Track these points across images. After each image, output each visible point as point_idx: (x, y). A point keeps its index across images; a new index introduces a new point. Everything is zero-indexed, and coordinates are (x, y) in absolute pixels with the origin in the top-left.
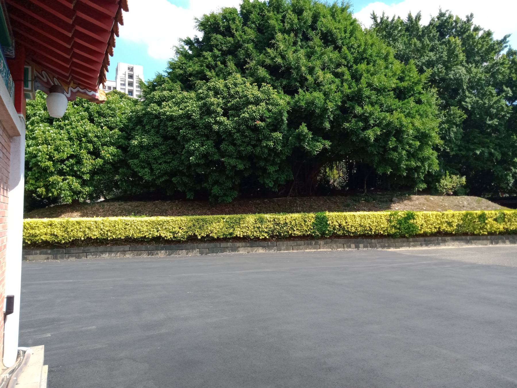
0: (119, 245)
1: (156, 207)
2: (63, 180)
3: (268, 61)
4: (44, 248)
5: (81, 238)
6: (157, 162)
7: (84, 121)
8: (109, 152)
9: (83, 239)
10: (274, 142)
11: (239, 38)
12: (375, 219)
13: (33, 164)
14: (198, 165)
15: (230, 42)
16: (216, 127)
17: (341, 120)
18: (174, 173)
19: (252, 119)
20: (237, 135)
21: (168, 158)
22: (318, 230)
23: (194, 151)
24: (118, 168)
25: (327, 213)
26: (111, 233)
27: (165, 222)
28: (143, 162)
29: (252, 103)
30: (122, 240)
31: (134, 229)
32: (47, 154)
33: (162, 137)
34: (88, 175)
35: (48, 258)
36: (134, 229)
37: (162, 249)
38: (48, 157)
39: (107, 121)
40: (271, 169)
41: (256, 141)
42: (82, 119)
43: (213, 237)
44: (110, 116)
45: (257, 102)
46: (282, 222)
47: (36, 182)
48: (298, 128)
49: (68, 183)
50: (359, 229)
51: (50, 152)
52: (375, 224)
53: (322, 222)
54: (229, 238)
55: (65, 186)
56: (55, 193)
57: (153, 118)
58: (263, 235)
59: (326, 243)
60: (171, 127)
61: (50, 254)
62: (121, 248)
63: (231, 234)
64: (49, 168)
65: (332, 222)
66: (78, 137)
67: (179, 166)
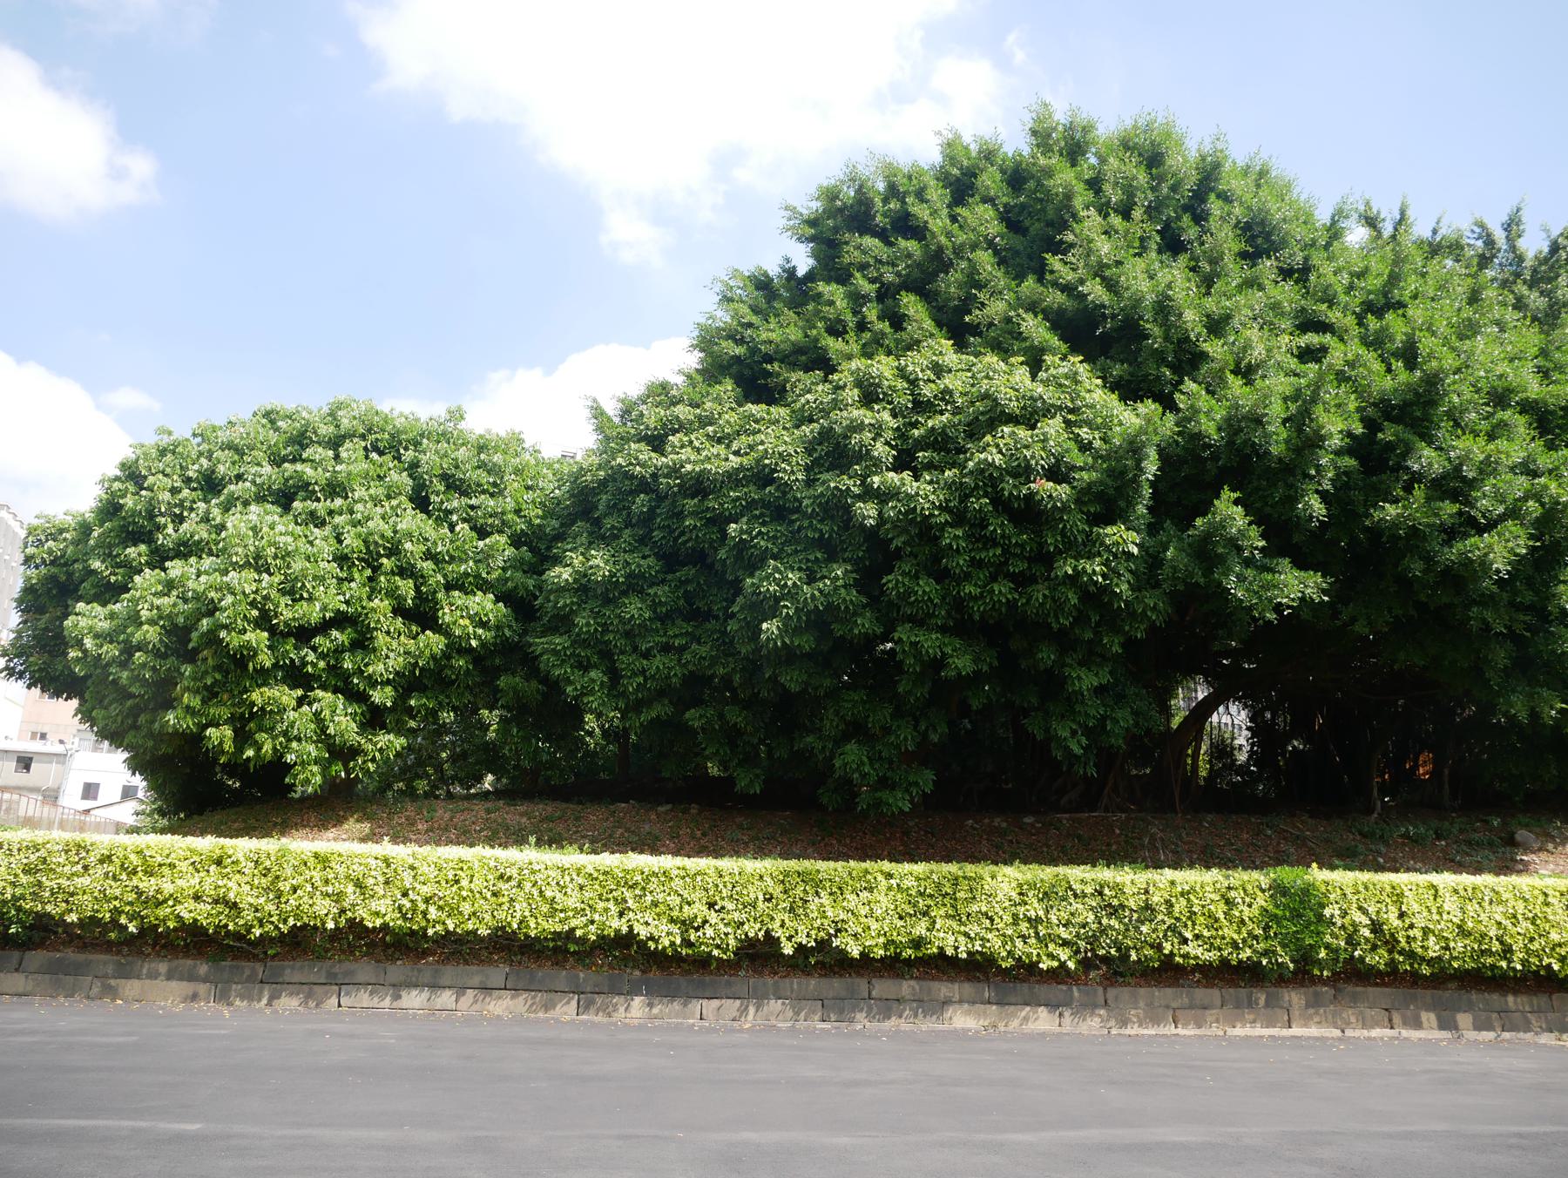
0: (467, 963)
1: (619, 824)
2: (301, 702)
3: (1056, 298)
4: (186, 951)
5: (324, 923)
6: (635, 649)
7: (394, 502)
8: (472, 613)
9: (330, 925)
10: (1106, 564)
11: (943, 239)
12: (1520, 906)
13: (203, 635)
14: (787, 656)
15: (909, 256)
16: (868, 512)
17: (1358, 496)
18: (695, 688)
19: (1015, 474)
20: (953, 536)
21: (677, 632)
22: (1284, 946)
23: (777, 600)
24: (496, 672)
25: (1318, 875)
26: (440, 908)
27: (655, 874)
28: (585, 644)
29: (1013, 420)
30: (482, 939)
31: (530, 897)
32: (253, 604)
33: (658, 556)
34: (388, 689)
35: (194, 997)
36: (530, 897)
37: (633, 992)
38: (255, 613)
39: (472, 507)
40: (1086, 680)
41: (1029, 560)
42: (389, 497)
43: (842, 953)
44: (484, 492)
45: (1030, 416)
46: (1132, 904)
47: (204, 702)
48: (1204, 508)
49: (317, 714)
50: (1459, 946)
51: (266, 598)
52: (1524, 926)
53: (1301, 909)
54: (908, 961)
55: (306, 725)
56: (267, 748)
57: (631, 492)
58: (1051, 956)
59: (1314, 1003)
60: (694, 514)
61: (205, 980)
62: (475, 974)
63: (917, 943)
64: (256, 654)
65: (1344, 914)
66: (369, 552)
67: (714, 661)
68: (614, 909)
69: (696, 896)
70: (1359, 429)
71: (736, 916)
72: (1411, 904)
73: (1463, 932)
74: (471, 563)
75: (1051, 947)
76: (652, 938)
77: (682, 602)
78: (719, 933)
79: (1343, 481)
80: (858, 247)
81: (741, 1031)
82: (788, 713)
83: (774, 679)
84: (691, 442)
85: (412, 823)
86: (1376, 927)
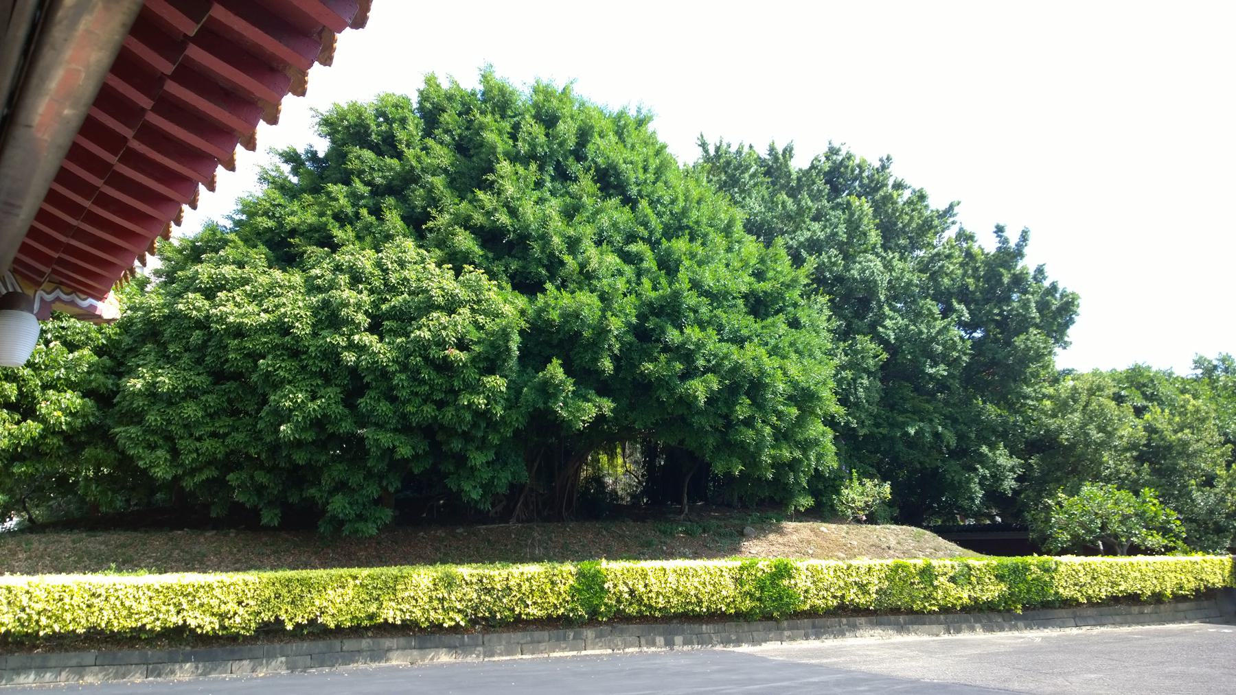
0: (66, 650)
3: (478, 218)
6: (191, 435)
8: (61, 406)
12: (708, 577)
14: (298, 444)
15: (392, 169)
17: (635, 356)
18: (231, 462)
19: (438, 344)
20: (400, 378)
21: (222, 425)
22: (582, 605)
23: (291, 411)
24: (82, 446)
25: (604, 565)
27: (202, 587)
28: (154, 432)
29: (439, 308)
30: (79, 635)
36: (113, 607)
39: (63, 328)
40: (478, 459)
45: (451, 307)
46: (498, 587)
50: (674, 601)
52: (709, 588)
53: (591, 584)
54: (366, 628)
58: (451, 619)
59: (600, 636)
60: (236, 350)
62: (74, 658)
63: (371, 617)
67: (247, 445)
68: (173, 610)
69: (229, 599)
70: (634, 320)
71: (256, 608)
72: (652, 579)
73: (678, 593)
74: (63, 370)
75: (451, 614)
76: (199, 626)
77: (225, 405)
78: (241, 619)
79: (627, 349)
80: (358, 157)
81: (257, 678)
82: (298, 476)
83: (289, 456)
84: (234, 298)
85: (13, 553)
86: (632, 592)
